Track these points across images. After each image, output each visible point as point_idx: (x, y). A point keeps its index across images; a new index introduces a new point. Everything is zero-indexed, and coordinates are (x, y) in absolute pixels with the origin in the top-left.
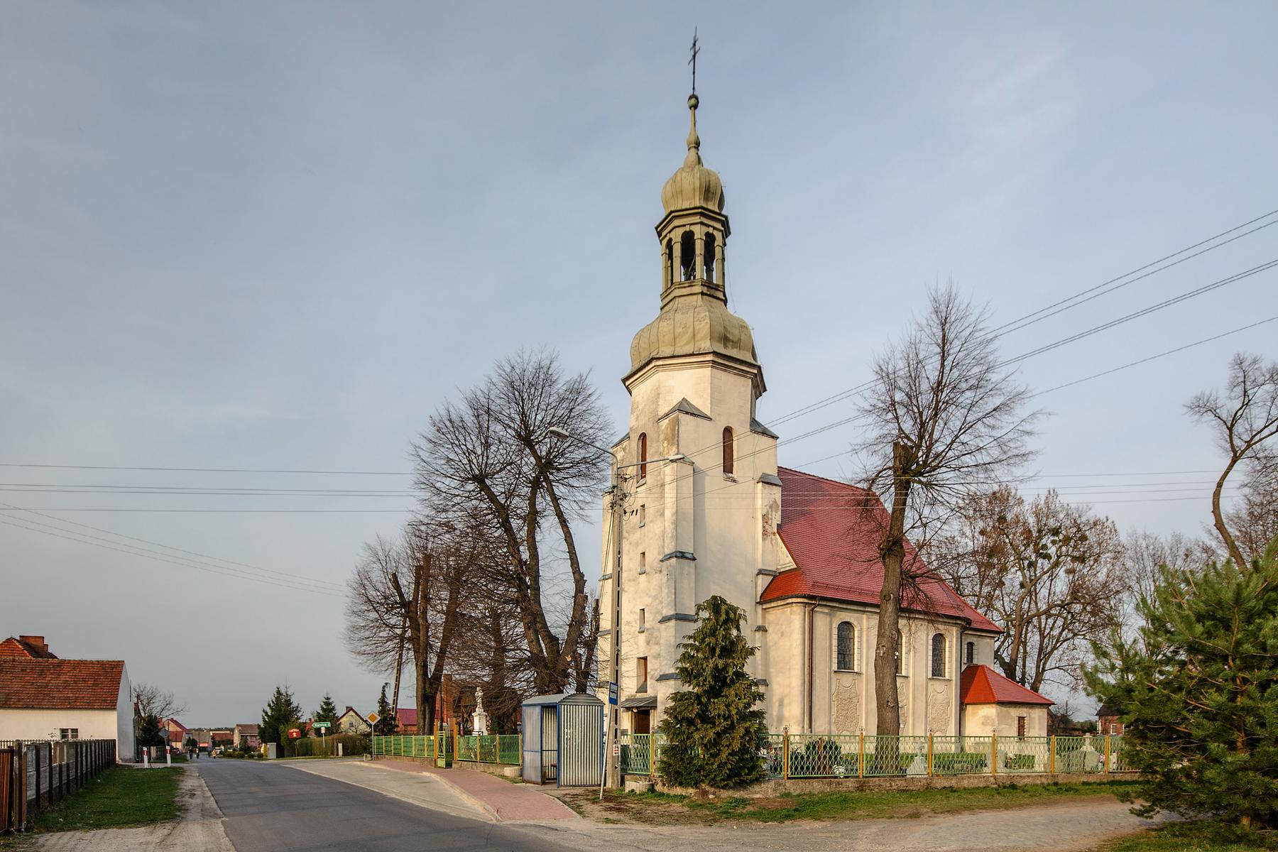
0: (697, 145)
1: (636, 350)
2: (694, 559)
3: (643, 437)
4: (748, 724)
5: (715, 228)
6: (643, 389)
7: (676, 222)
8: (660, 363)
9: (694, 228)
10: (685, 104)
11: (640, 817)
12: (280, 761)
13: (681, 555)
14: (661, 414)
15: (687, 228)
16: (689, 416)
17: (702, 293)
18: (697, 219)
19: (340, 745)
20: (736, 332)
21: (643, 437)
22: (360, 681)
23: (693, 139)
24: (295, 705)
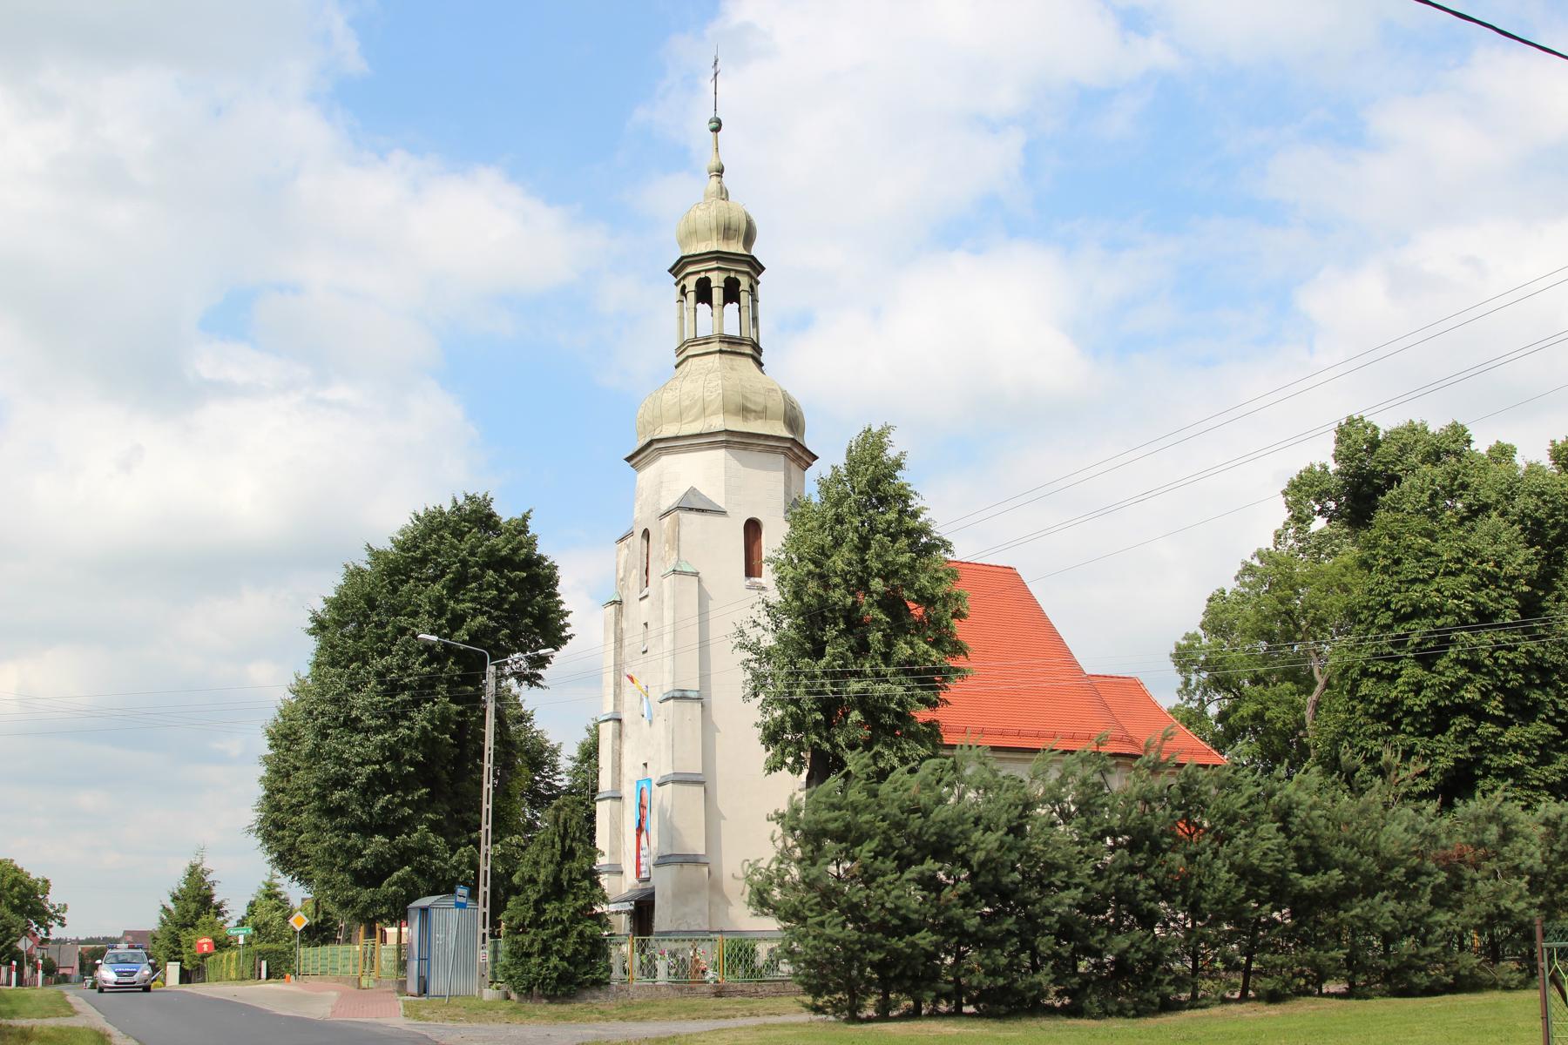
0: (720, 171)
4: (580, 927)
6: (649, 474)
8: (662, 445)
9: (709, 275)
12: (188, 988)
14: (664, 509)
15: (703, 275)
17: (721, 352)
18: (714, 265)
19: (264, 964)
22: (244, 873)
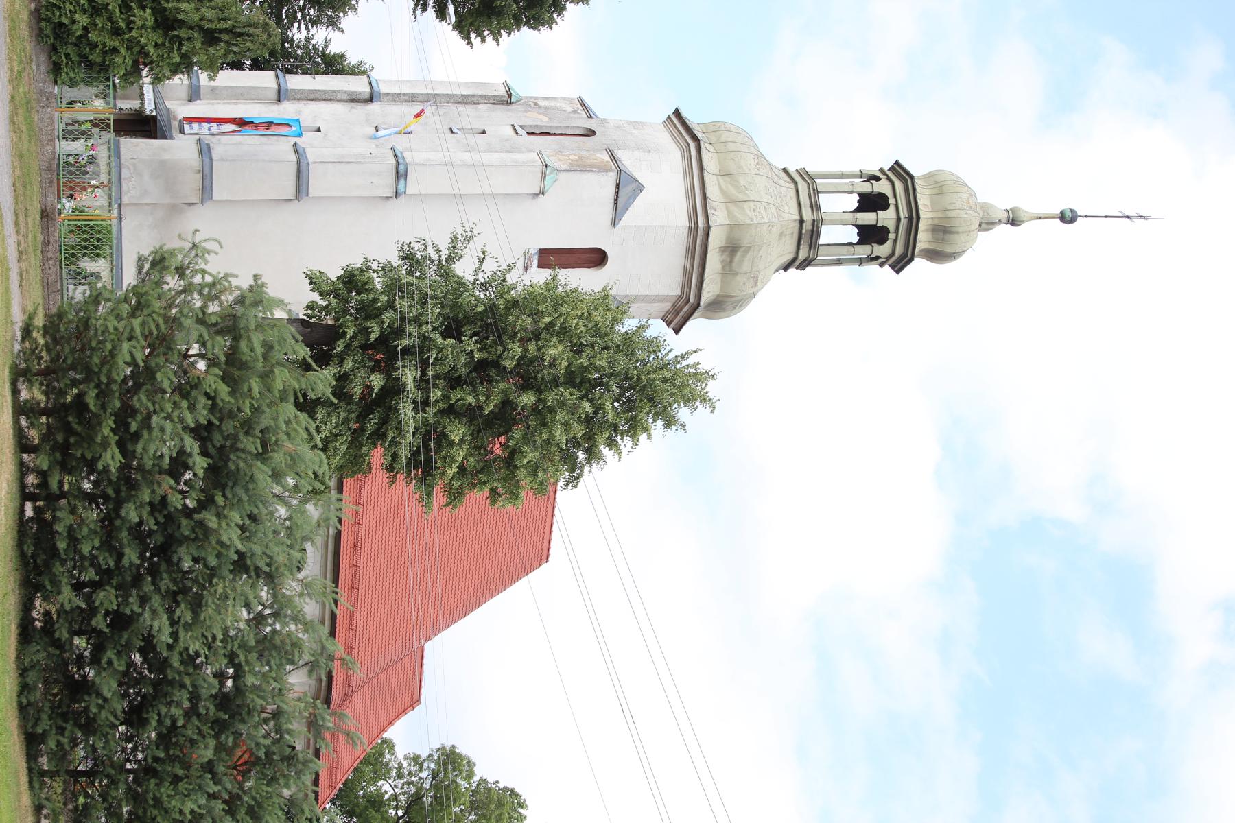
1: (714, 128)
2: (397, 195)
3: (590, 133)
5: (895, 241)
7: (899, 186)
8: (693, 152)
9: (892, 209)
10: (1065, 206)
11: (30, 770)
13: (400, 175)
14: (620, 154)
15: (891, 201)
16: (613, 189)
18: (904, 214)
20: (746, 267)
21: (590, 133)
23: (1021, 215)
24: (683, 413)
